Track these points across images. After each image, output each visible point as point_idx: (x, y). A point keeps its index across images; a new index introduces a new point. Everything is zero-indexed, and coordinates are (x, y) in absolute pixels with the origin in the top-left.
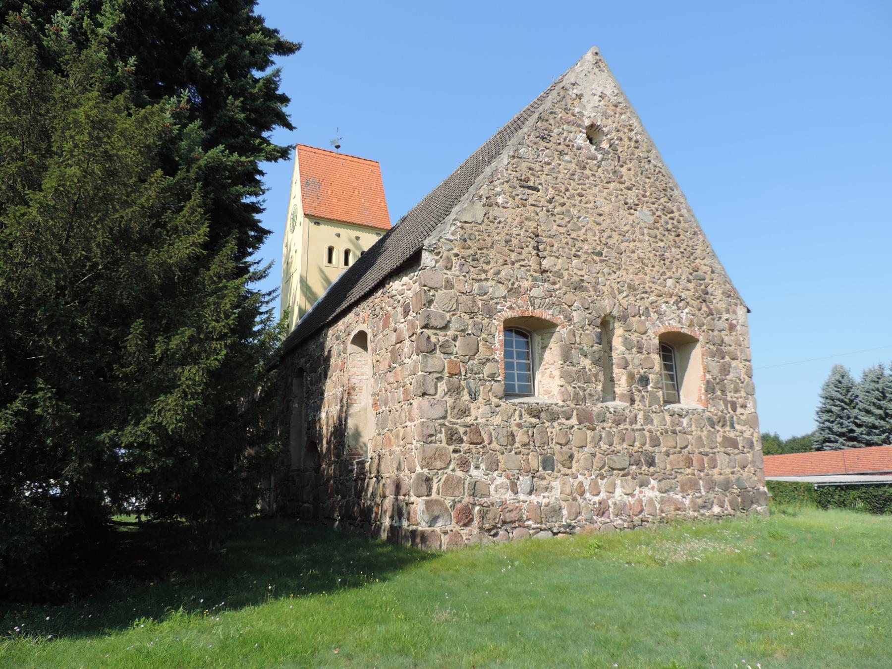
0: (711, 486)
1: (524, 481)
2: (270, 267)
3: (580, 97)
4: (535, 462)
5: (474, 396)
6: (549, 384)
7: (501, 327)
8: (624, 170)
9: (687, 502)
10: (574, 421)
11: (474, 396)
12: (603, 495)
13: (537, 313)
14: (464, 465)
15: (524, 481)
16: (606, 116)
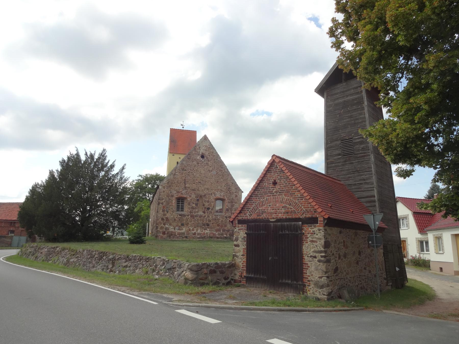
0: (224, 230)
1: (177, 228)
2: (123, 168)
3: (200, 147)
4: (180, 224)
5: (167, 212)
6: (187, 209)
7: (33, 243)
8: (209, 163)
9: (217, 233)
10: (189, 217)
11: (167, 212)
12: (195, 231)
13: (183, 196)
14: (164, 224)
15: (177, 228)
16: (206, 150)
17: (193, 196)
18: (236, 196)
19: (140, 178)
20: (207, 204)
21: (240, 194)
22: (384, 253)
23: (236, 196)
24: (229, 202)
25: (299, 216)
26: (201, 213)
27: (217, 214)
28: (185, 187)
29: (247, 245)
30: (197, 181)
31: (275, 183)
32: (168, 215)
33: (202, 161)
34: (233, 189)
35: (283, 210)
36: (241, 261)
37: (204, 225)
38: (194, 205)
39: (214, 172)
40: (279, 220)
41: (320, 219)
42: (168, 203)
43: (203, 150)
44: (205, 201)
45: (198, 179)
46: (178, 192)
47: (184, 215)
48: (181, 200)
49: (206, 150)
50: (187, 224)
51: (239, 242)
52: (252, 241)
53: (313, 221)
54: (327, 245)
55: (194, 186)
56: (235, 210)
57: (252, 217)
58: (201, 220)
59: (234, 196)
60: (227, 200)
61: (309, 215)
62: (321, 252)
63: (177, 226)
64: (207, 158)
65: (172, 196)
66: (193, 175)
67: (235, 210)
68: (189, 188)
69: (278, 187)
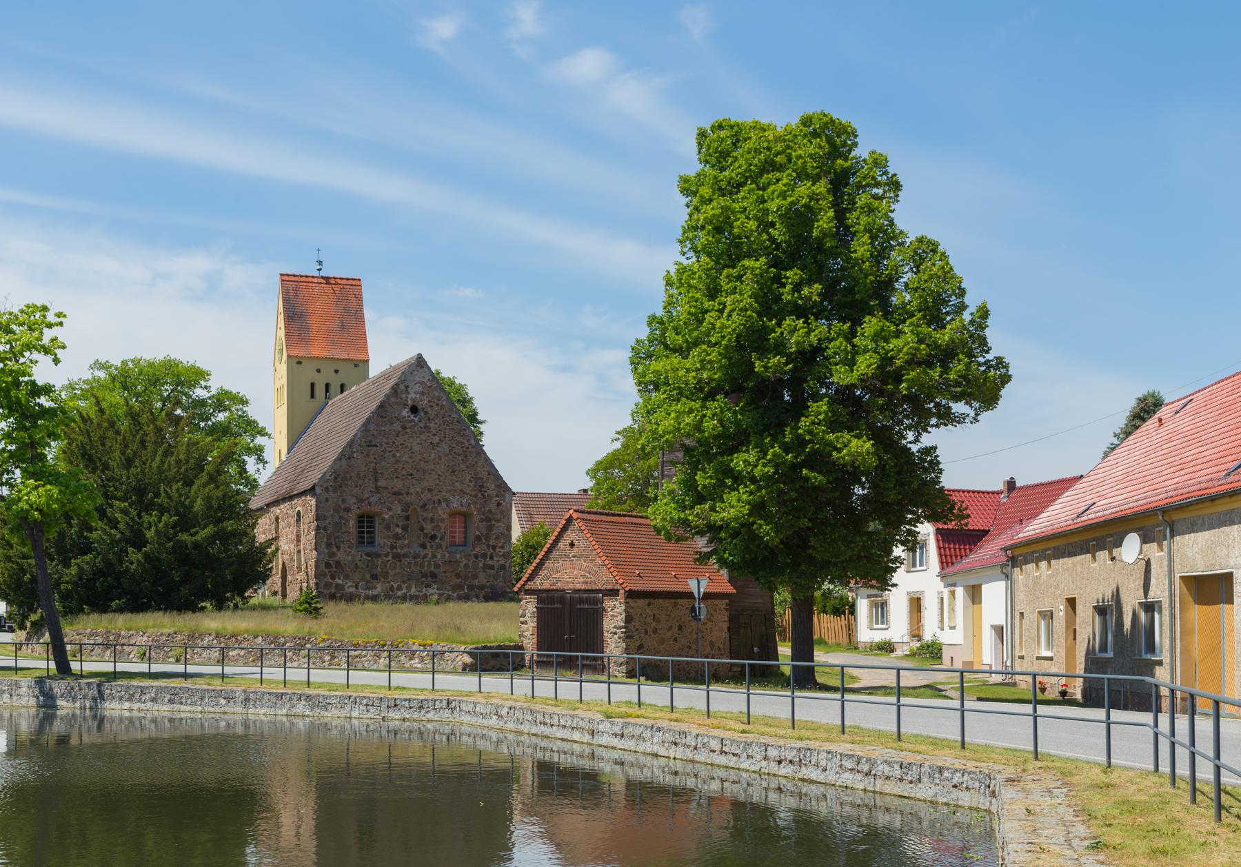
3: (407, 387)
4: (368, 577)
5: (338, 548)
6: (381, 539)
11: (338, 548)
14: (333, 577)
16: (422, 393)
17: (397, 509)
18: (499, 504)
19: (101, 374)
20: (428, 527)
21: (507, 500)
22: (729, 629)
23: (499, 504)
24: (481, 521)
25: (599, 587)
26: (416, 549)
27: (454, 549)
28: (377, 487)
29: (538, 622)
30: (404, 472)
31: (572, 545)
32: (340, 556)
33: (412, 421)
34: (491, 488)
35: (582, 580)
36: (530, 643)
37: (425, 576)
38: (399, 530)
39: (444, 448)
40: (576, 591)
41: (622, 591)
42: (338, 526)
43: (416, 393)
44: (425, 520)
45: (406, 466)
46: (361, 500)
47: (378, 555)
48: (366, 521)
49: (422, 393)
50: (386, 575)
51: (526, 618)
52: (541, 614)
53: (613, 593)
54: (628, 619)
55: (398, 485)
56: (497, 539)
57: (544, 587)
58: (416, 564)
59: (493, 506)
60: (476, 516)
61: (610, 587)
62: (621, 628)
63: (362, 580)
64: (426, 413)
65: (348, 510)
66: (394, 456)
67: (497, 539)
68: (386, 488)
69: (575, 550)
